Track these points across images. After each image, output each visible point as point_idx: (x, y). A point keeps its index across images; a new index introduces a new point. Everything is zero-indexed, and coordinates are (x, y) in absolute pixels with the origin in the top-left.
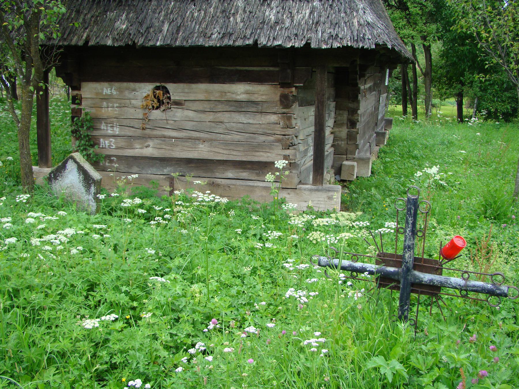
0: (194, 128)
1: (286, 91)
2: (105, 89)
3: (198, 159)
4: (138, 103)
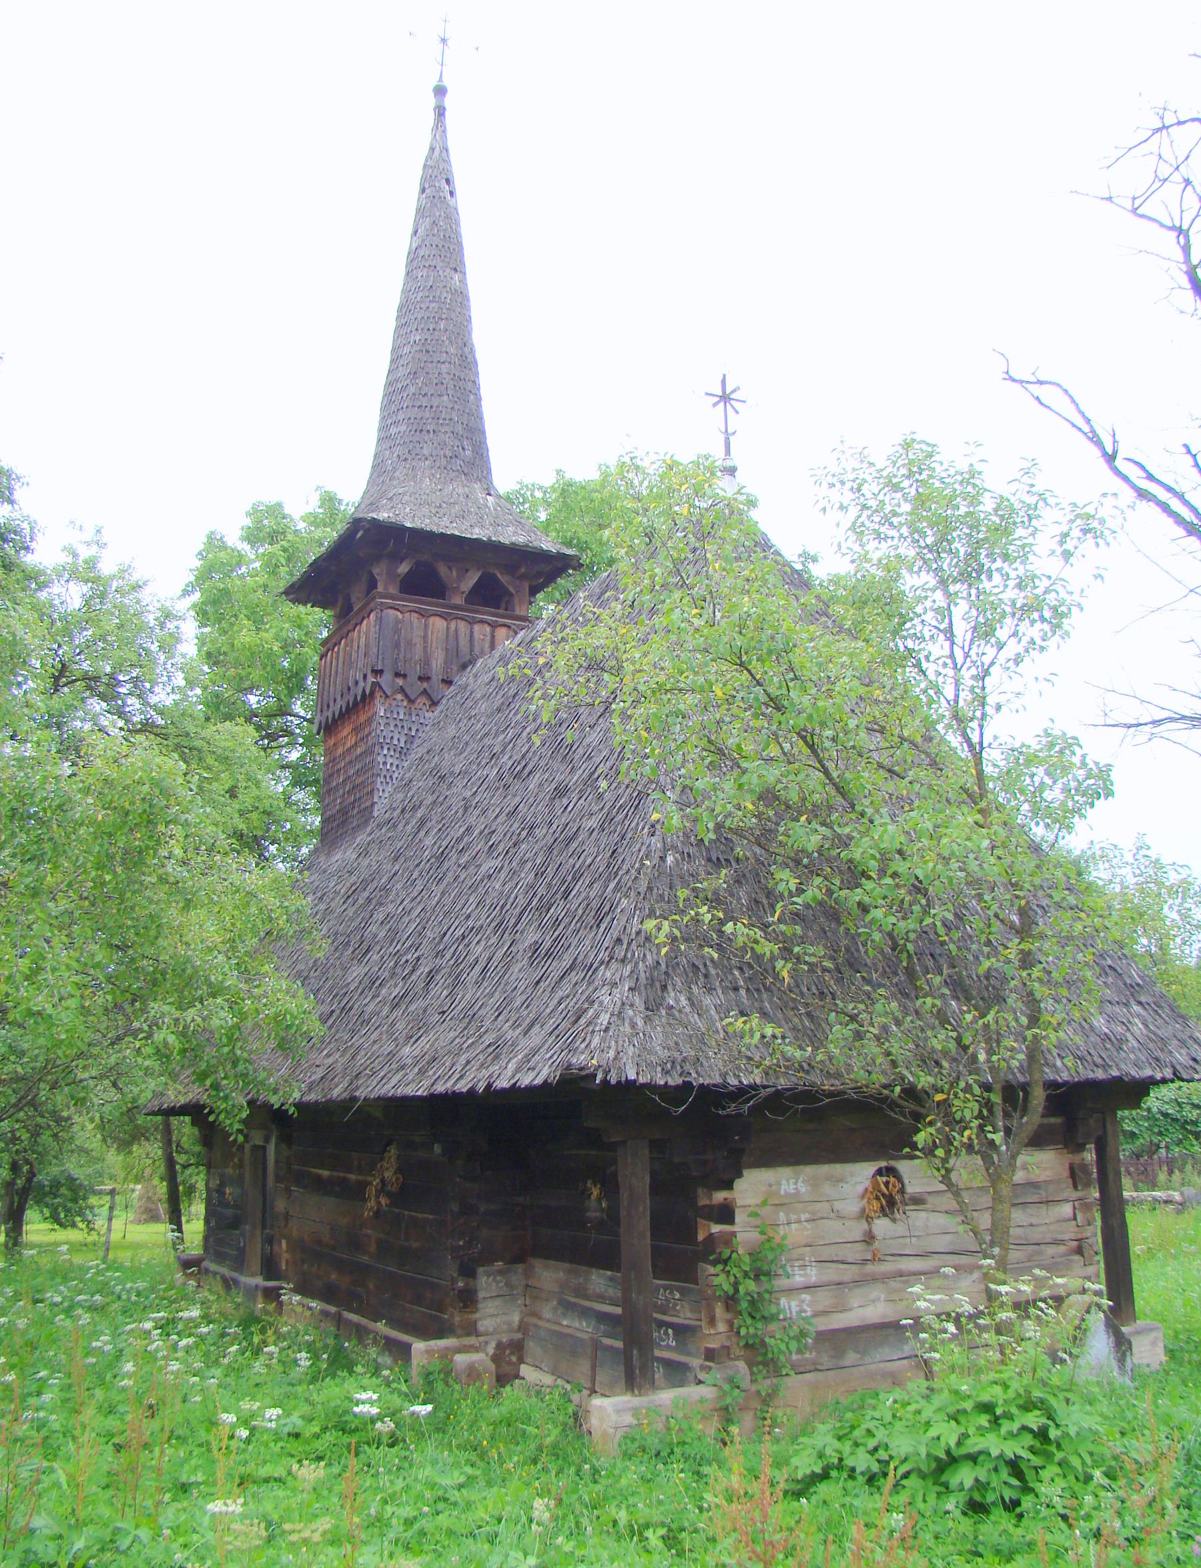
0: (957, 1248)
1: (1076, 1159)
2: (784, 1182)
3: (859, 1327)
4: (852, 1206)
